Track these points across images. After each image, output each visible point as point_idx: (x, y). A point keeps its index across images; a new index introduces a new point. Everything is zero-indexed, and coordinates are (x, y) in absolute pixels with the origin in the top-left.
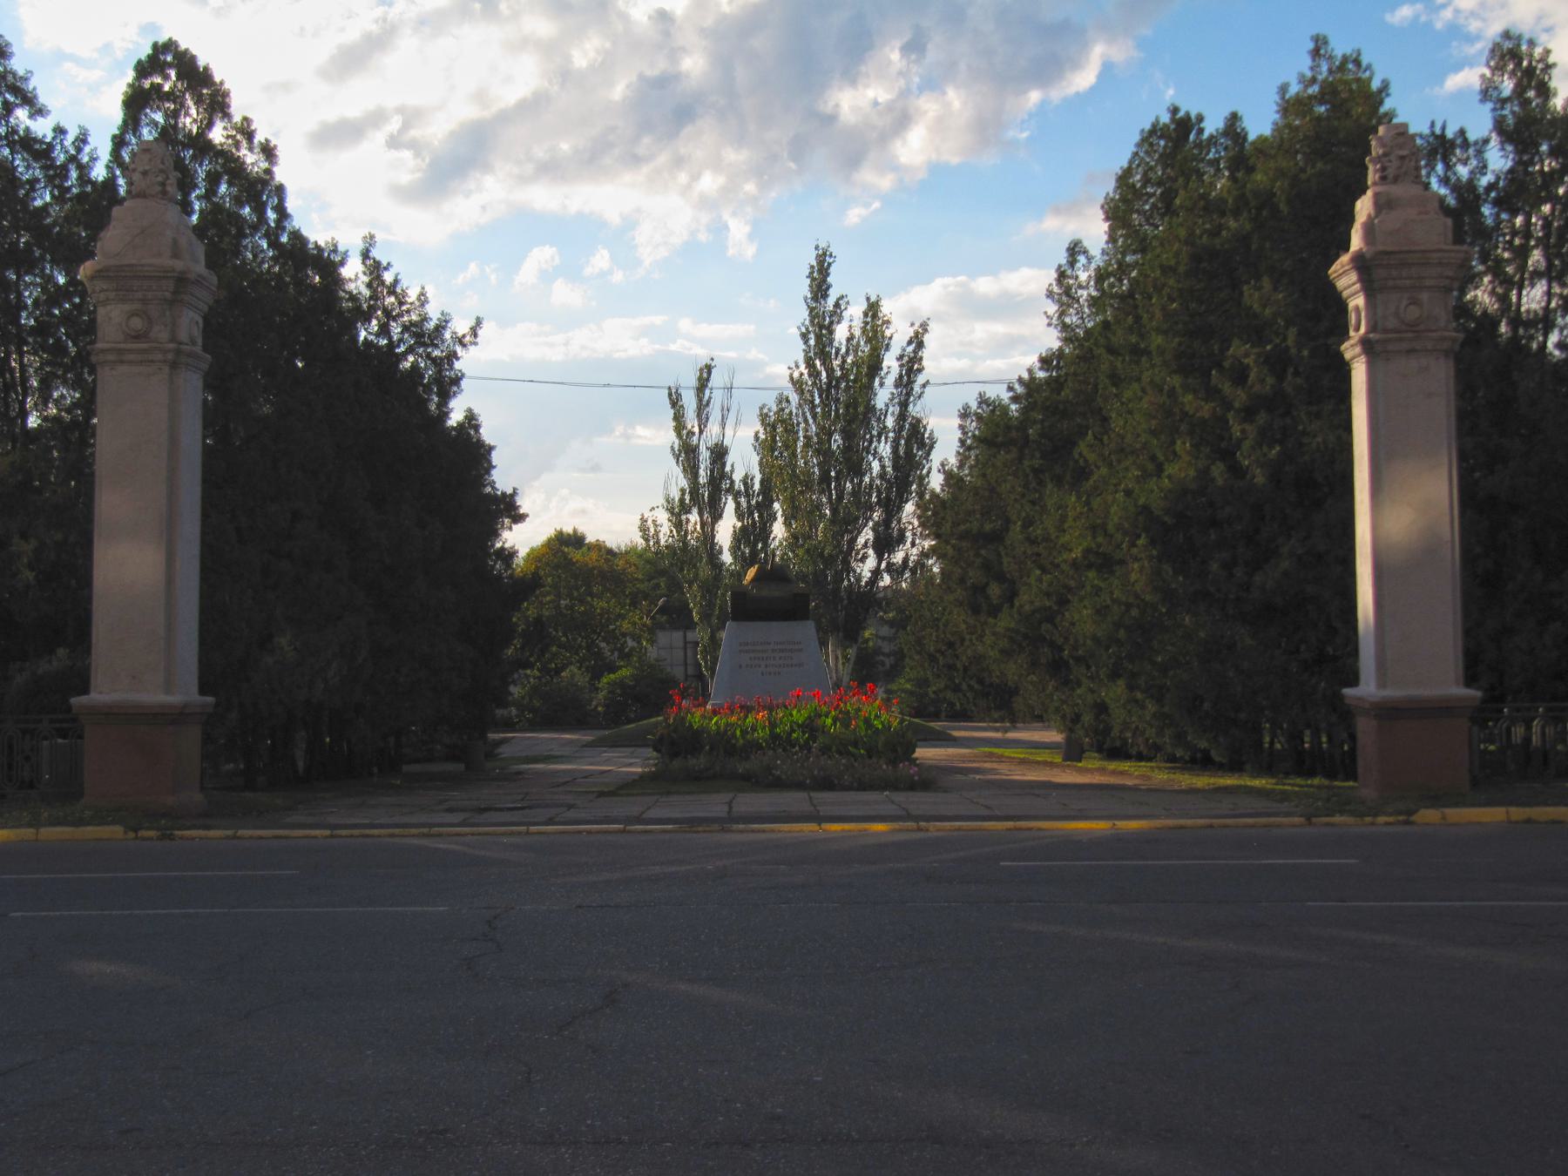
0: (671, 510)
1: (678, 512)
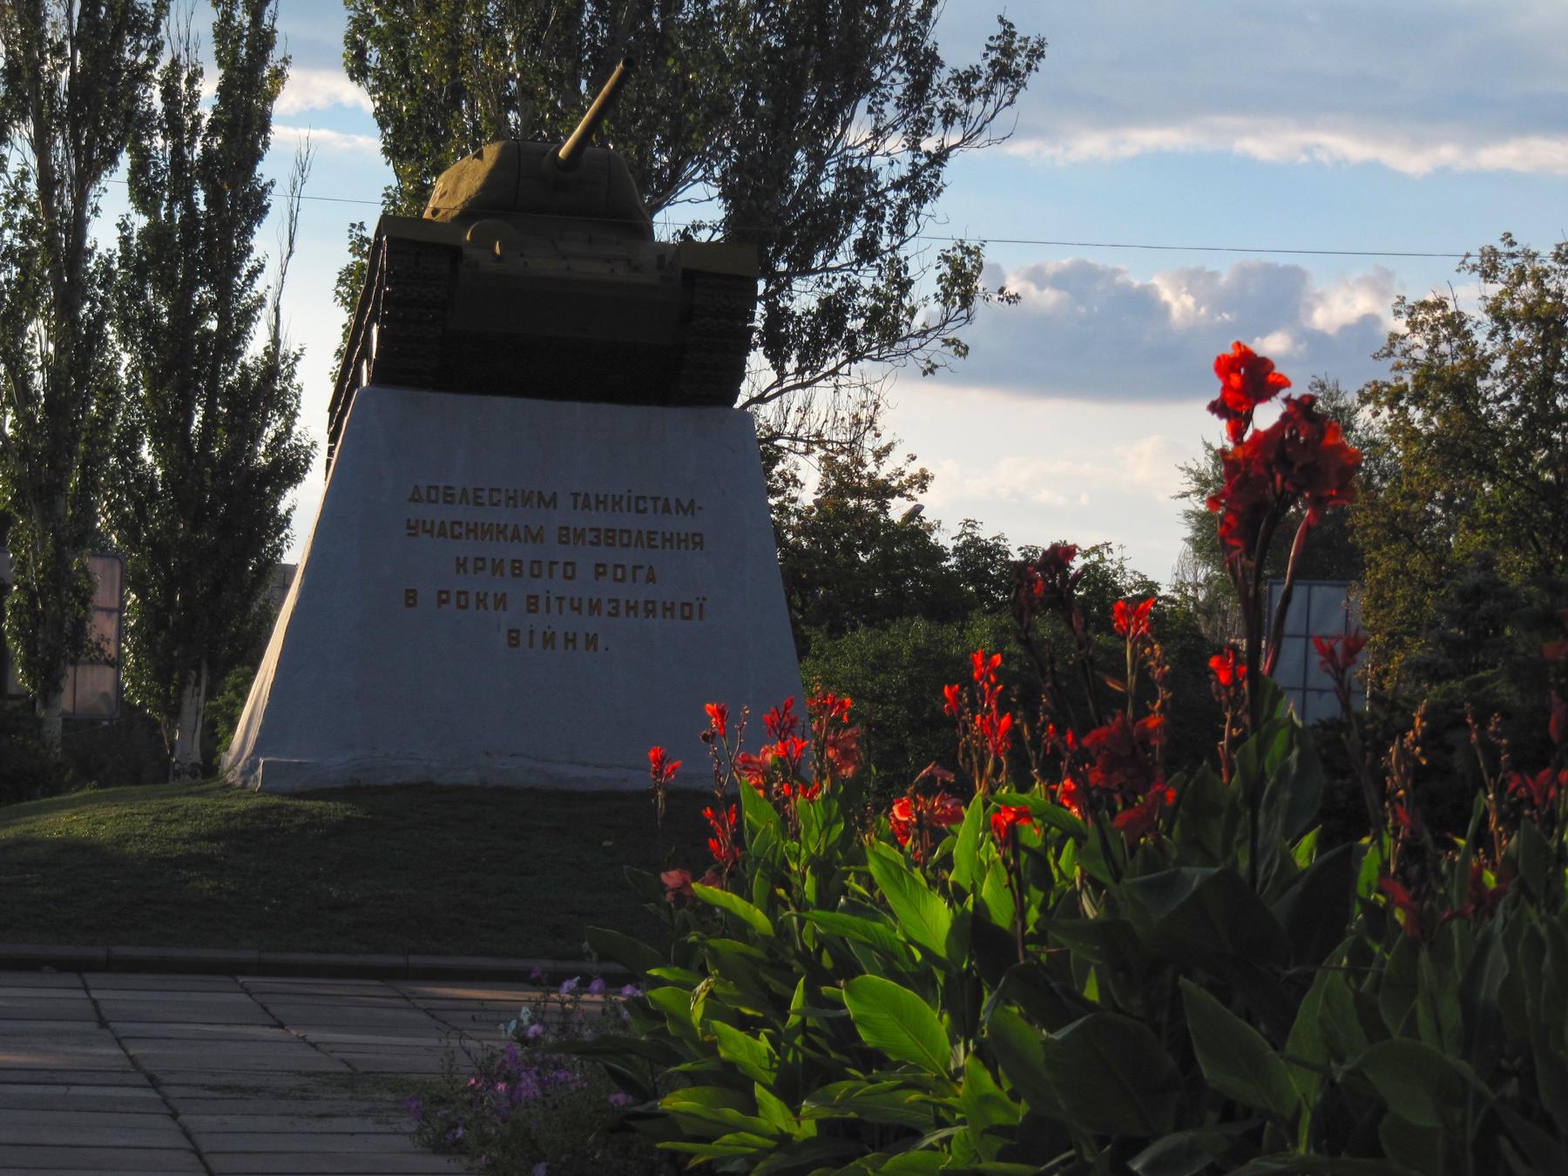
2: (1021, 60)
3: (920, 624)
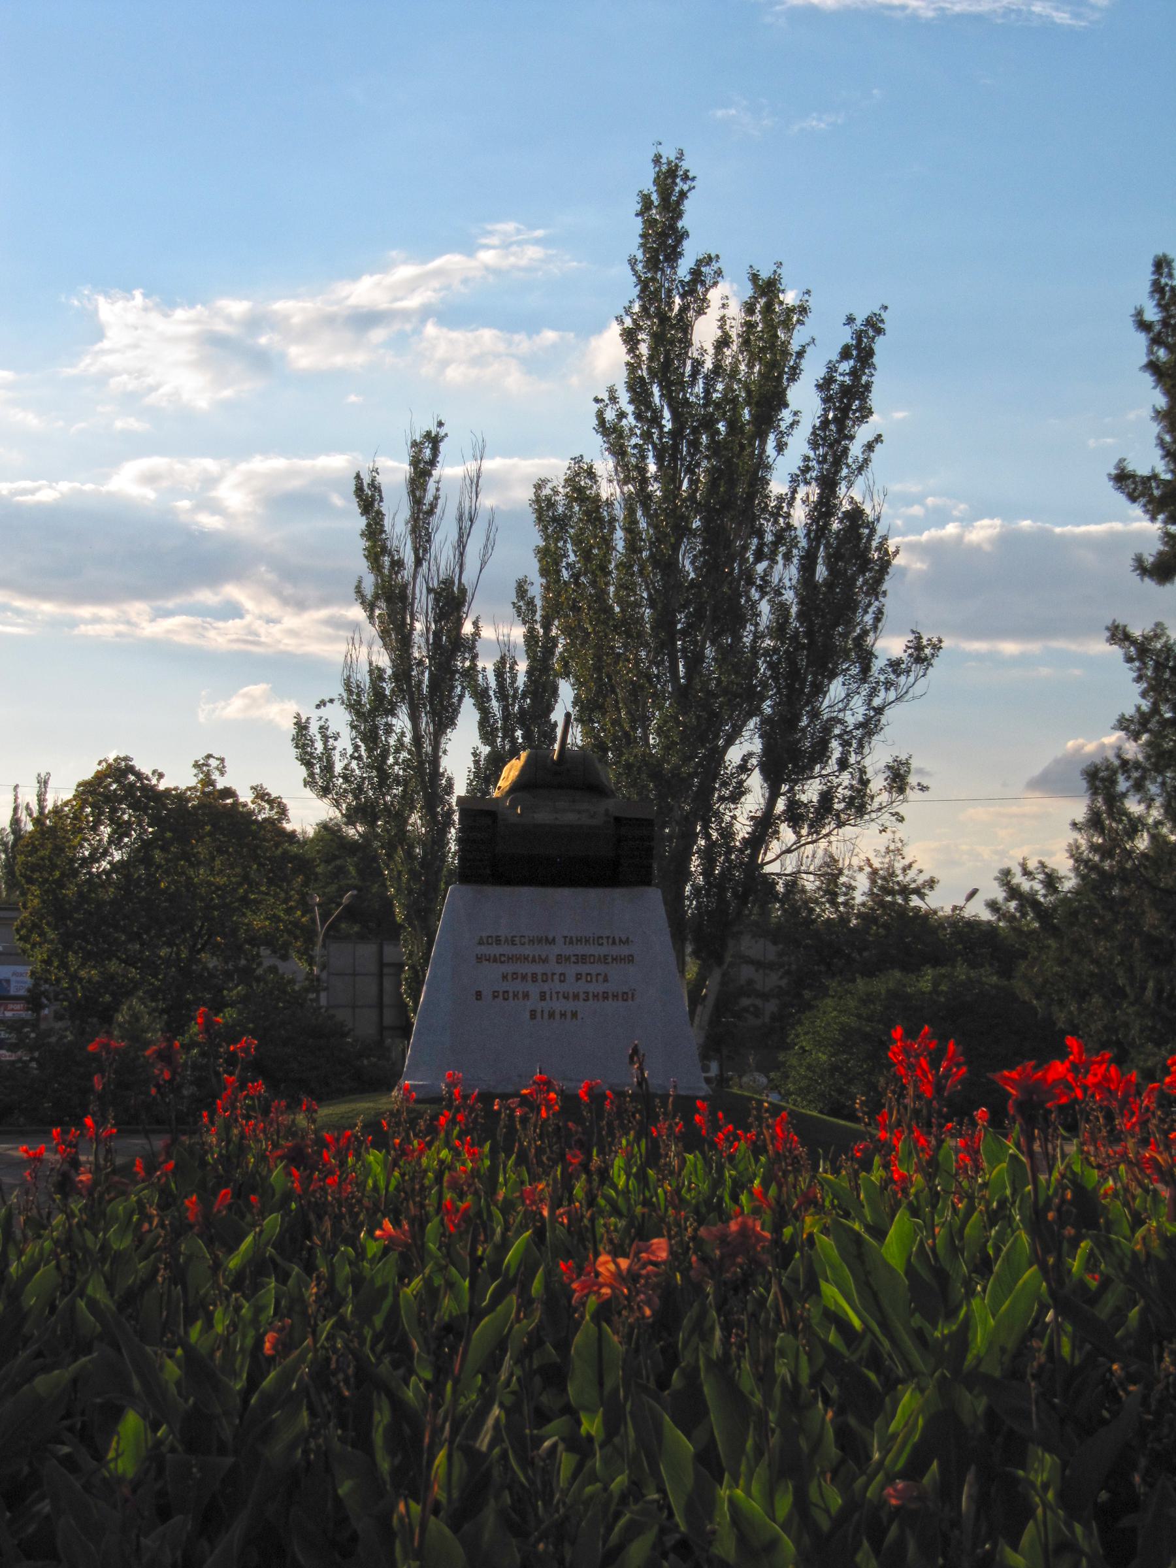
0: (354, 707)
1: (369, 712)
2: (928, 651)
3: (897, 974)
